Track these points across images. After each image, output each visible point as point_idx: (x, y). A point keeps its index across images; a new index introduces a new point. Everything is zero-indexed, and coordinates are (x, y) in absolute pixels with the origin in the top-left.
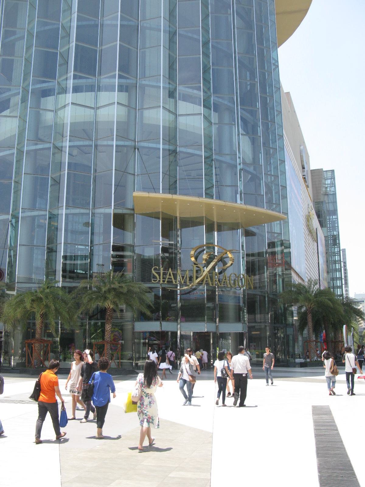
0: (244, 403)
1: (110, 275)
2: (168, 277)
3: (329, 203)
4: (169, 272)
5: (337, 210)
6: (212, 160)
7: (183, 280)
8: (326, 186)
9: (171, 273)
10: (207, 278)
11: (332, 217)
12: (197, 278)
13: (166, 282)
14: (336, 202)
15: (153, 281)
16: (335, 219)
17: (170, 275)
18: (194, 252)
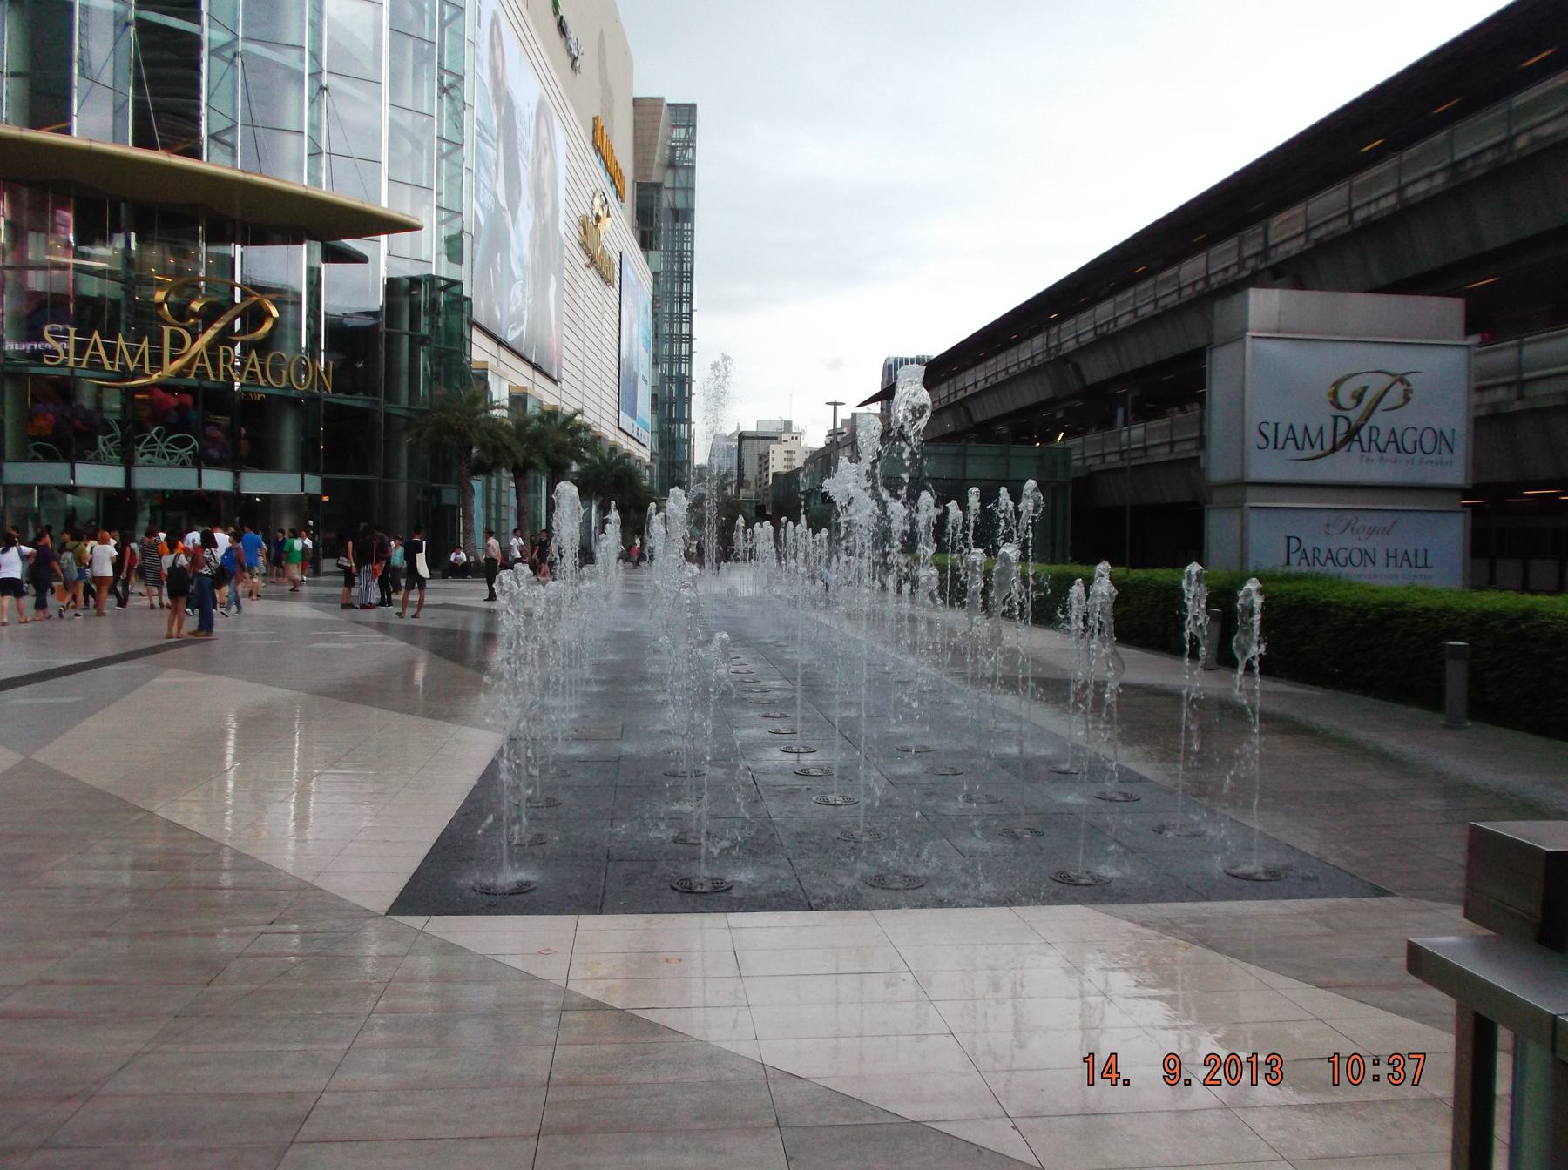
0: (116, 490)
1: (409, 677)
2: (89, 352)
3: (677, 192)
4: (92, 340)
5: (693, 210)
6: (235, 55)
7: (132, 362)
8: (673, 144)
9: (99, 341)
10: (202, 360)
11: (683, 226)
12: (173, 359)
13: (84, 365)
14: (693, 189)
15: (46, 362)
16: (687, 230)
17: (95, 348)
18: (164, 293)
